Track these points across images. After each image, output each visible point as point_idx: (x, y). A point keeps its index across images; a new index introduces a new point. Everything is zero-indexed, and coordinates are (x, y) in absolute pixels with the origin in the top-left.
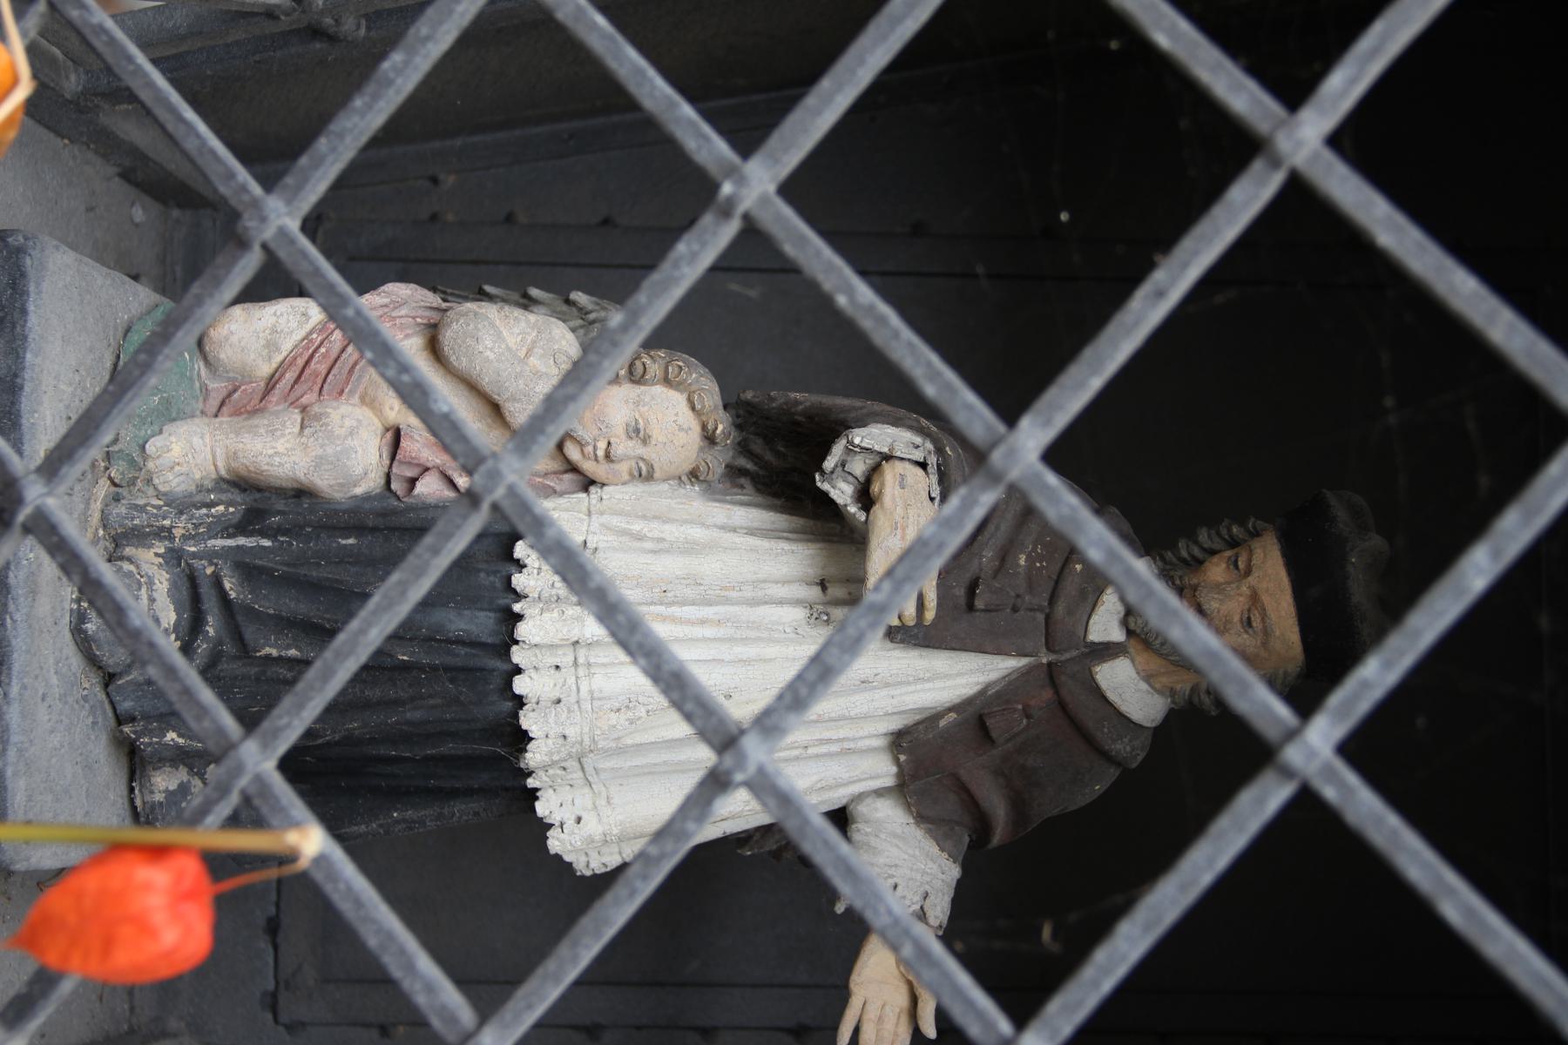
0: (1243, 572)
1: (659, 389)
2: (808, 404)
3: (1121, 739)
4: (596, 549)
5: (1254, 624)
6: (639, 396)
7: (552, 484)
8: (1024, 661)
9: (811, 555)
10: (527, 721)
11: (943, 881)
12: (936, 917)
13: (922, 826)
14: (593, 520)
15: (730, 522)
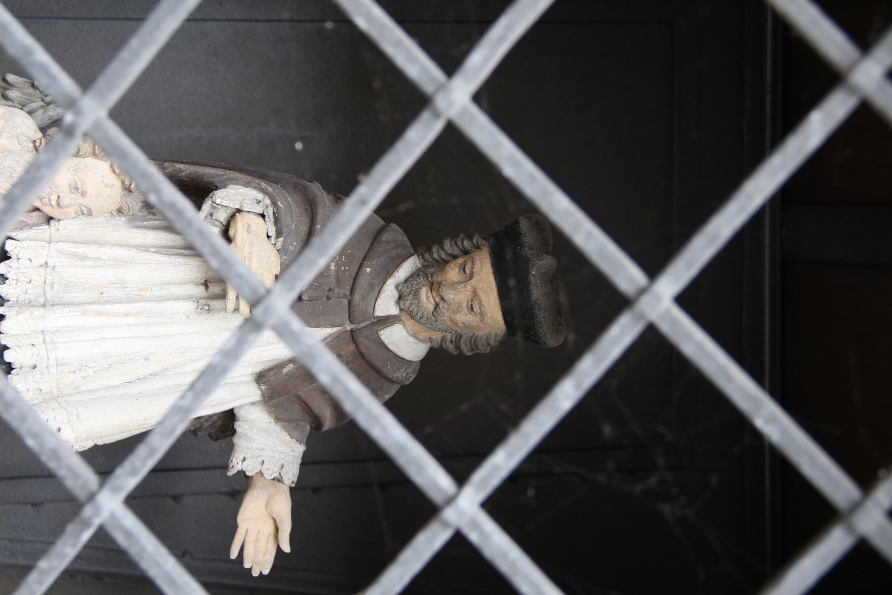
0: (468, 275)
1: (90, 160)
2: (188, 172)
3: (399, 370)
4: (55, 267)
5: (475, 310)
6: (76, 165)
7: (25, 220)
11: (293, 456)
12: (289, 479)
13: (279, 424)
14: (51, 247)
15: (146, 241)
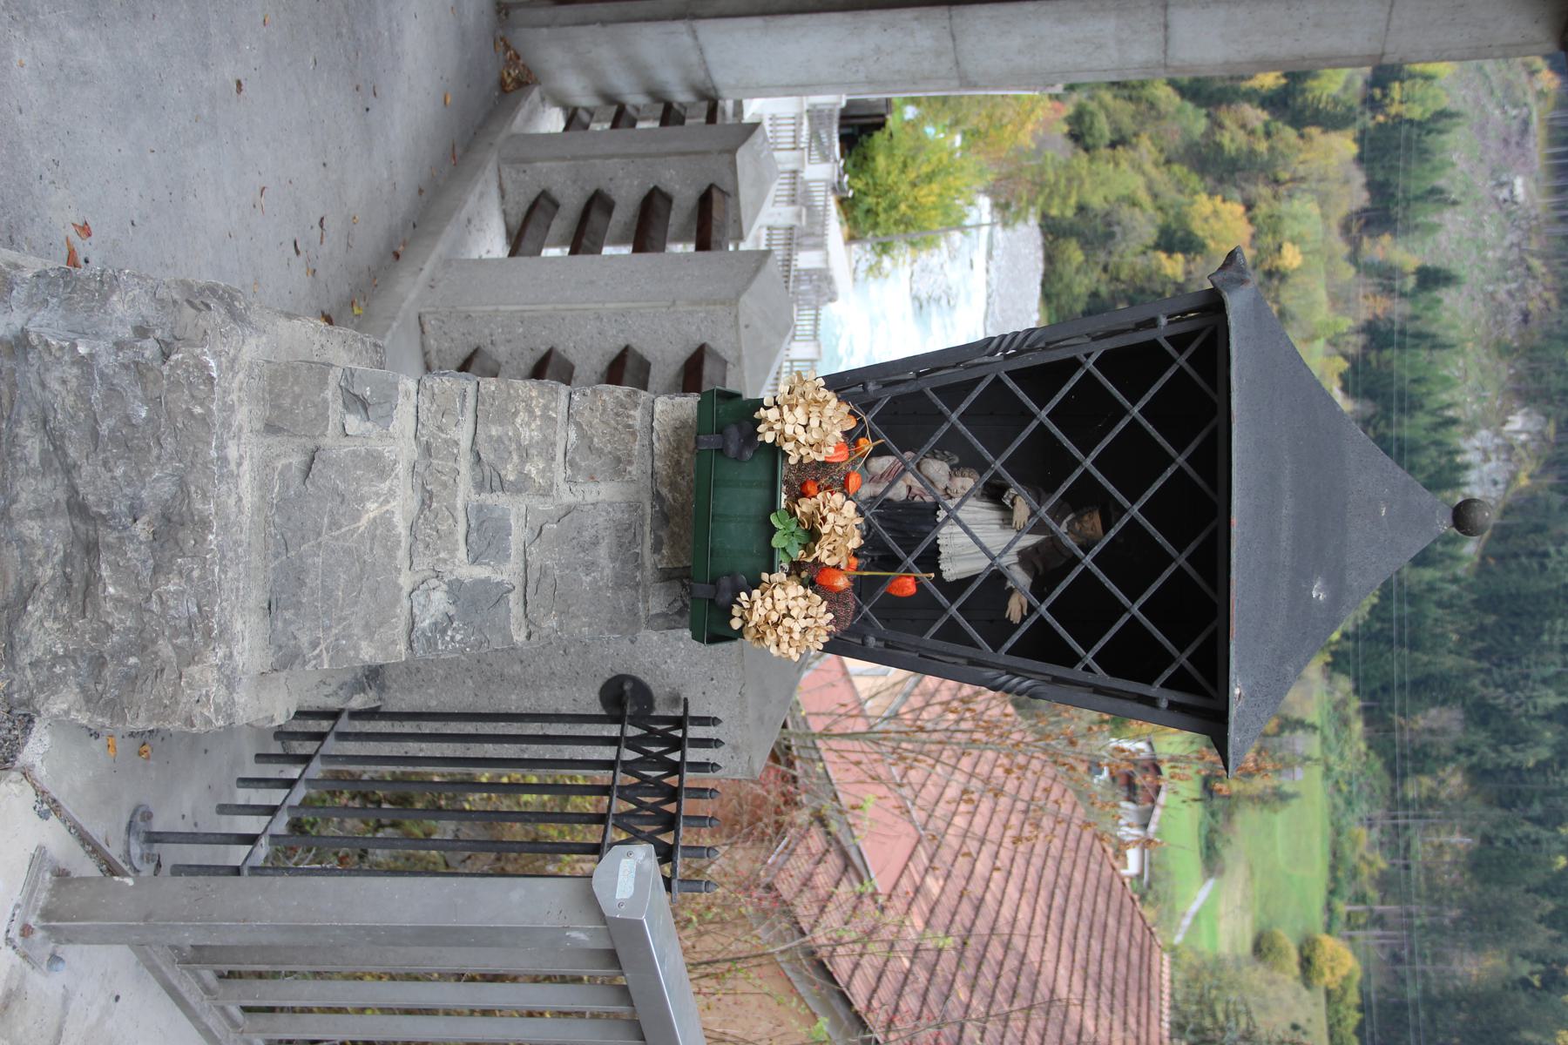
8: (1042, 537)
9: (1319, 101)
10: (941, 549)
